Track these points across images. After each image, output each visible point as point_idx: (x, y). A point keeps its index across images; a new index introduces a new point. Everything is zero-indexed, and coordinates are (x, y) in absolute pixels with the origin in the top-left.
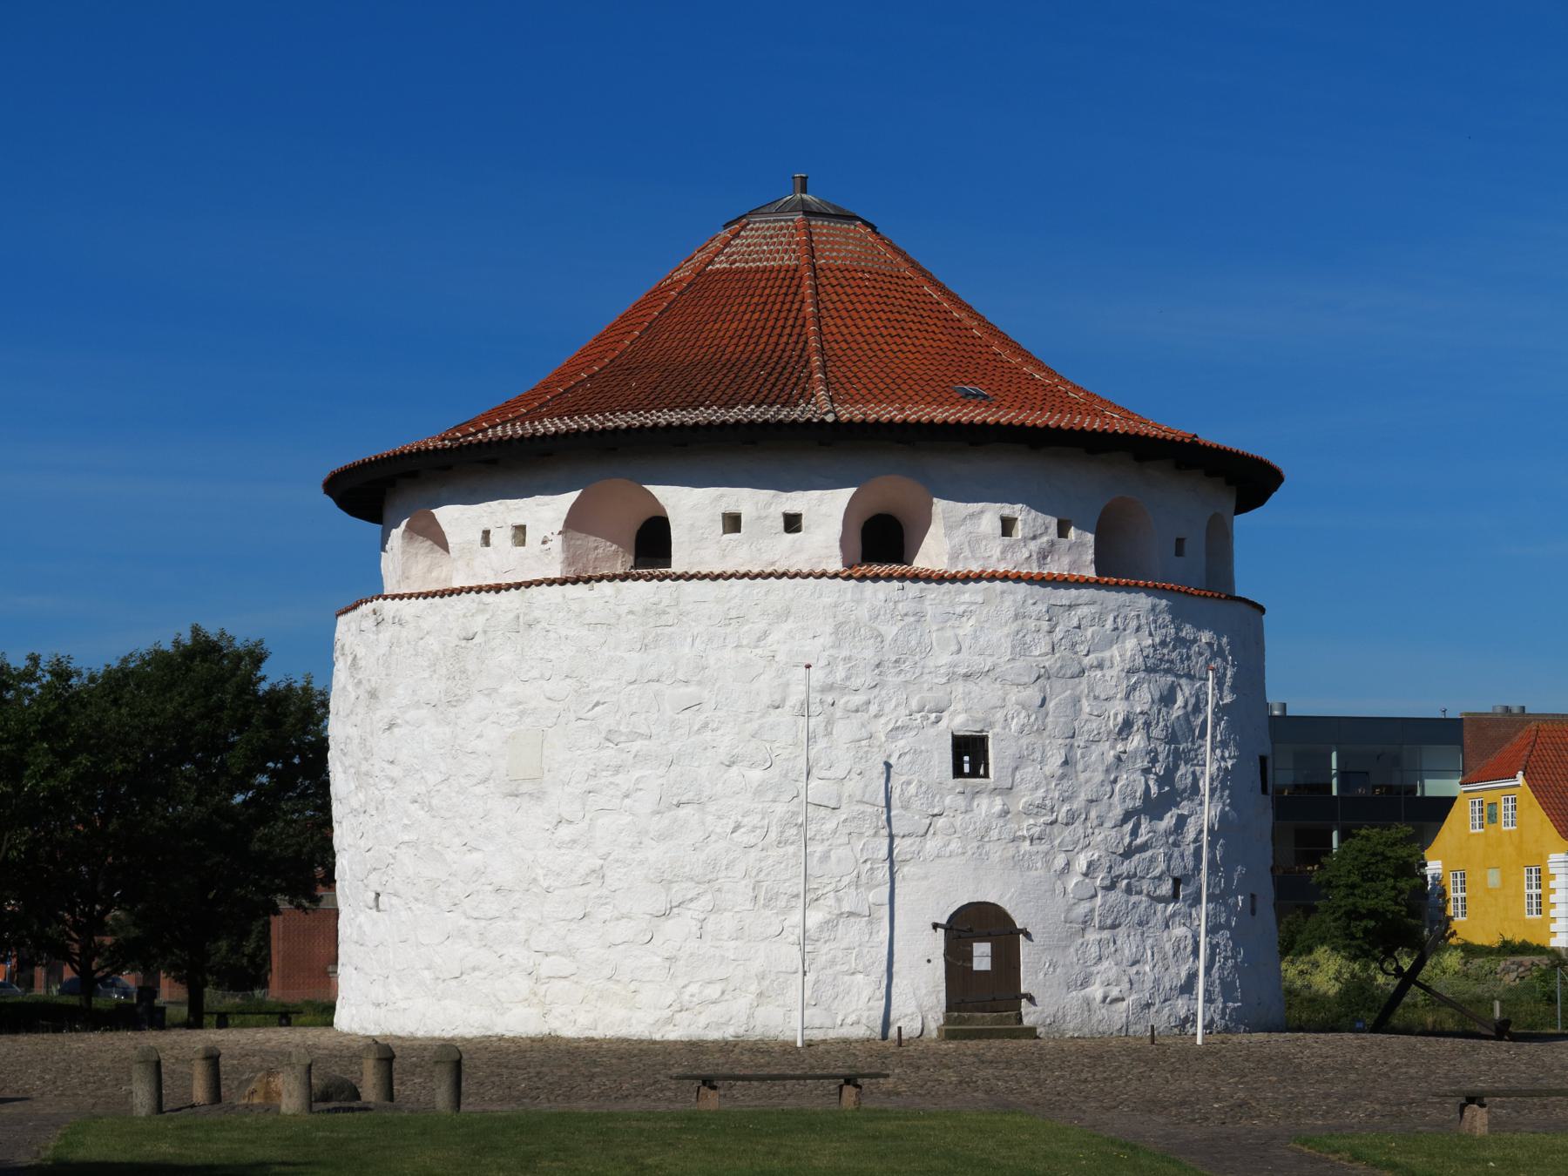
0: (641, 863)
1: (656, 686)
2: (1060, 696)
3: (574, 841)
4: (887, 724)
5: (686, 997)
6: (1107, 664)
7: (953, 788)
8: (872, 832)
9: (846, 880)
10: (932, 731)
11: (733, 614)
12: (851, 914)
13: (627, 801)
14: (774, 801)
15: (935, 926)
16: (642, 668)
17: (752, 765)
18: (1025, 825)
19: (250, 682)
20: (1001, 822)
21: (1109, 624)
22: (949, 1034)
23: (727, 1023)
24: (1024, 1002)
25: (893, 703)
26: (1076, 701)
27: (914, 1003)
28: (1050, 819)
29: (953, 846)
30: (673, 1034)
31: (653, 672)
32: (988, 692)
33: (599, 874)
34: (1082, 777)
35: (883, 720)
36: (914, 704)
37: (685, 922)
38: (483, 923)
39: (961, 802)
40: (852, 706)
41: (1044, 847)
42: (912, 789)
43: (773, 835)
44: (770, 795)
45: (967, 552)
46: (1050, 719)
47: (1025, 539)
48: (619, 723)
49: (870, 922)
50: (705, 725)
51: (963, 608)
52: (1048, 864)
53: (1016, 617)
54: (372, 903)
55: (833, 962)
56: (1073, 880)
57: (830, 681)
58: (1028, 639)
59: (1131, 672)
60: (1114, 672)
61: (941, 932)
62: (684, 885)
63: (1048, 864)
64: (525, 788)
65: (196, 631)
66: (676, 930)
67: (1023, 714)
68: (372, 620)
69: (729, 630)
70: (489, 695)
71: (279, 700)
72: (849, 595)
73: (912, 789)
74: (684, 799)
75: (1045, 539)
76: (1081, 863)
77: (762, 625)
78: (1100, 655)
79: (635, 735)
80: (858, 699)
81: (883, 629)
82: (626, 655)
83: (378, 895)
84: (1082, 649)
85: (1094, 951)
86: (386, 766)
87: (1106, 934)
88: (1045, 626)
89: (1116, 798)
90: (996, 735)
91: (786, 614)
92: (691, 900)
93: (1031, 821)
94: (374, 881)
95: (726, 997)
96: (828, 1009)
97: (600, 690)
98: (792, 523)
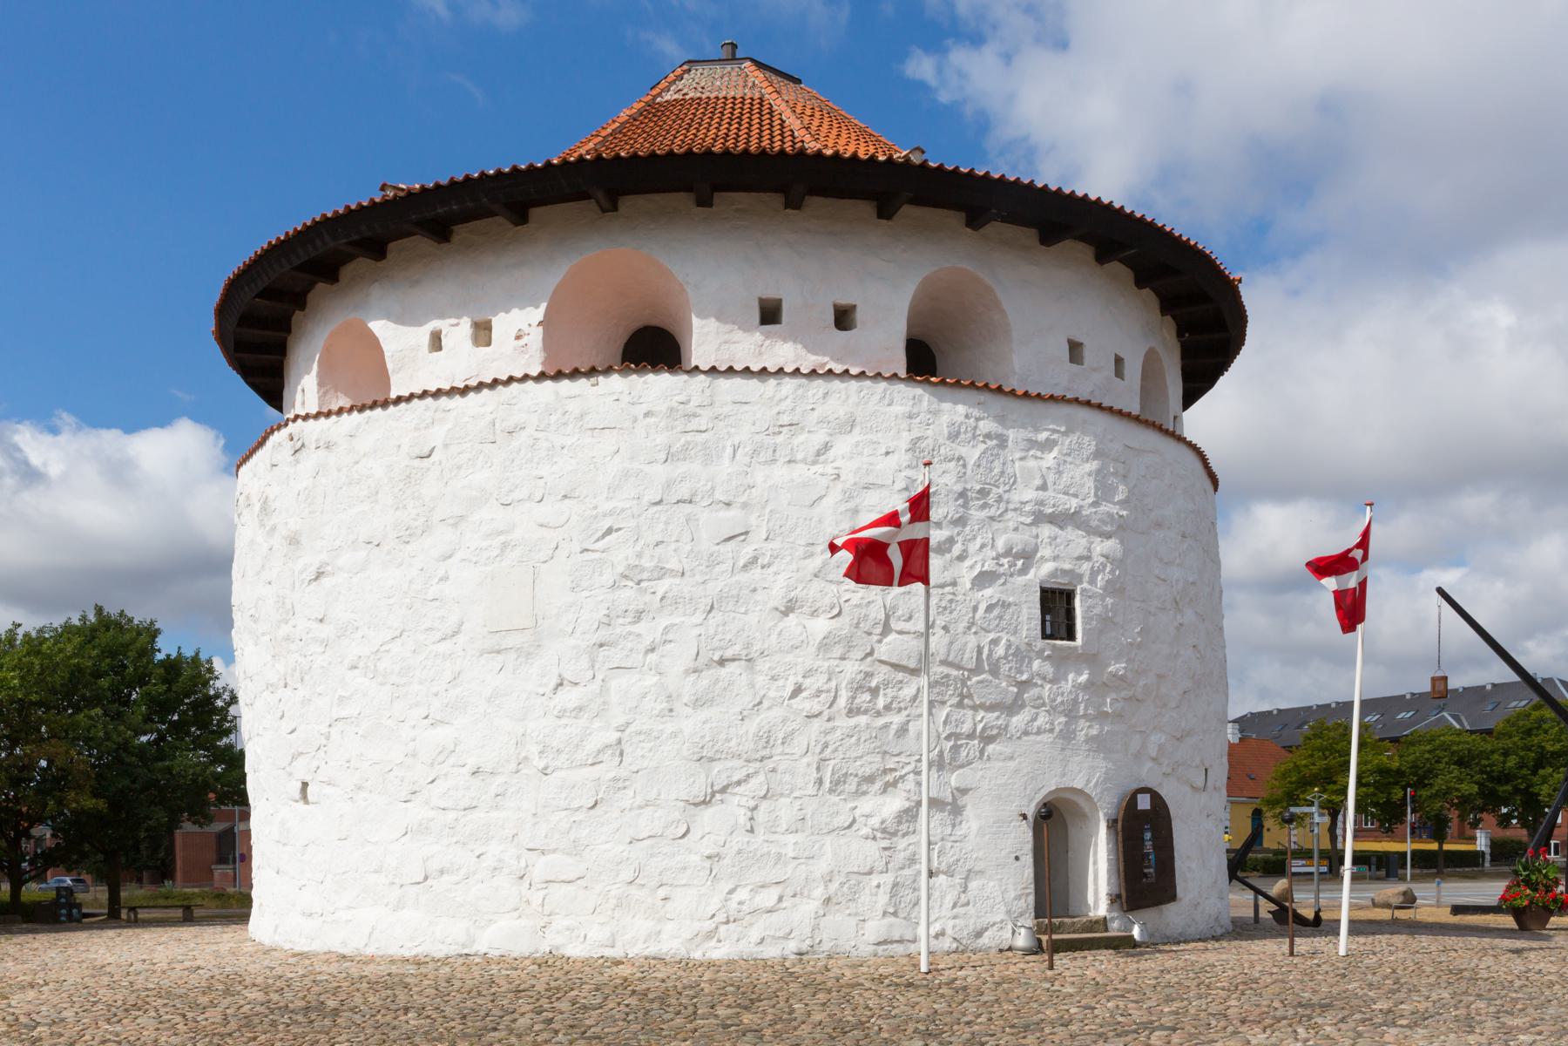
0: (674, 735)
1: (687, 508)
3: (580, 709)
4: (972, 567)
5: (733, 905)
7: (1043, 651)
8: (955, 700)
10: (1021, 580)
11: (785, 419)
13: (652, 657)
14: (843, 658)
16: (668, 485)
17: (814, 613)
19: (148, 651)
23: (786, 937)
25: (979, 542)
27: (1003, 909)
31: (684, 491)
32: (1076, 540)
33: (619, 749)
35: (968, 563)
37: (734, 807)
38: (452, 815)
39: (1049, 669)
43: (842, 702)
44: (838, 651)
48: (639, 555)
50: (754, 560)
54: (297, 795)
62: (729, 764)
64: (513, 640)
65: (99, 610)
68: (288, 447)
69: (779, 439)
70: (455, 525)
71: (173, 667)
72: (925, 404)
74: (729, 654)
77: (819, 438)
79: (661, 572)
82: (647, 468)
83: (305, 785)
86: (315, 625)
90: (1084, 590)
91: (850, 424)
92: (739, 783)
94: (301, 771)
95: (783, 905)
97: (611, 513)
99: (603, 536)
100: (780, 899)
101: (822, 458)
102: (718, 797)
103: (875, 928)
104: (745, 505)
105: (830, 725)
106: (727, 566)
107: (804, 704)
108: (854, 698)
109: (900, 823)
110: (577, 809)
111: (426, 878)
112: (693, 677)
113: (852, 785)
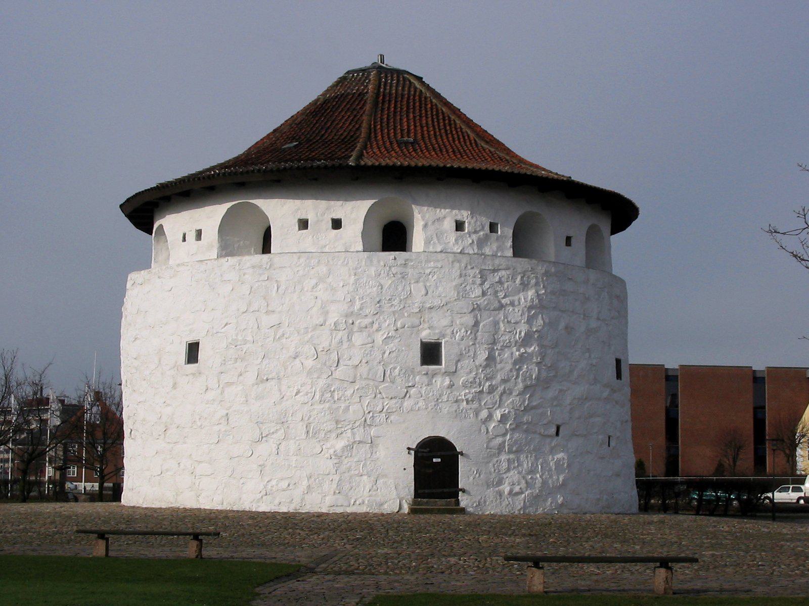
2: (486, 322)
3: (214, 400)
4: (383, 335)
6: (516, 303)
9: (357, 424)
12: (360, 442)
13: (241, 378)
15: (409, 449)
18: (463, 393)
20: (449, 391)
21: (518, 281)
22: (413, 511)
24: (460, 493)
26: (496, 324)
28: (478, 390)
29: (420, 404)
30: (263, 507)
34: (499, 366)
35: (381, 333)
36: (399, 325)
38: (171, 445)
39: (425, 379)
40: (363, 325)
41: (475, 405)
42: (397, 371)
43: (317, 397)
45: (435, 240)
46: (479, 333)
47: (469, 233)
49: (372, 447)
51: (429, 270)
52: (477, 414)
53: (461, 276)
55: (349, 470)
56: (492, 425)
57: (352, 310)
58: (468, 288)
59: (530, 308)
60: (521, 308)
61: (413, 452)
63: (477, 414)
66: (265, 449)
67: (463, 330)
73: (397, 371)
74: (270, 377)
75: (482, 233)
76: (498, 415)
78: (511, 298)
80: (367, 321)
81: (382, 282)
84: (501, 295)
85: (505, 465)
87: (512, 456)
88: (478, 281)
89: (520, 380)
92: (273, 433)
93: (467, 391)
96: (347, 495)
98: (337, 224)
99: (225, 326)
100: (289, 485)
101: (314, 290)
102: (264, 439)
103: (329, 500)
104: (280, 312)
105: (313, 407)
106: (271, 339)
107: (300, 398)
108: (323, 395)
109: (343, 452)
110: (212, 444)
111: (161, 473)
112: (256, 386)
113: (322, 435)
